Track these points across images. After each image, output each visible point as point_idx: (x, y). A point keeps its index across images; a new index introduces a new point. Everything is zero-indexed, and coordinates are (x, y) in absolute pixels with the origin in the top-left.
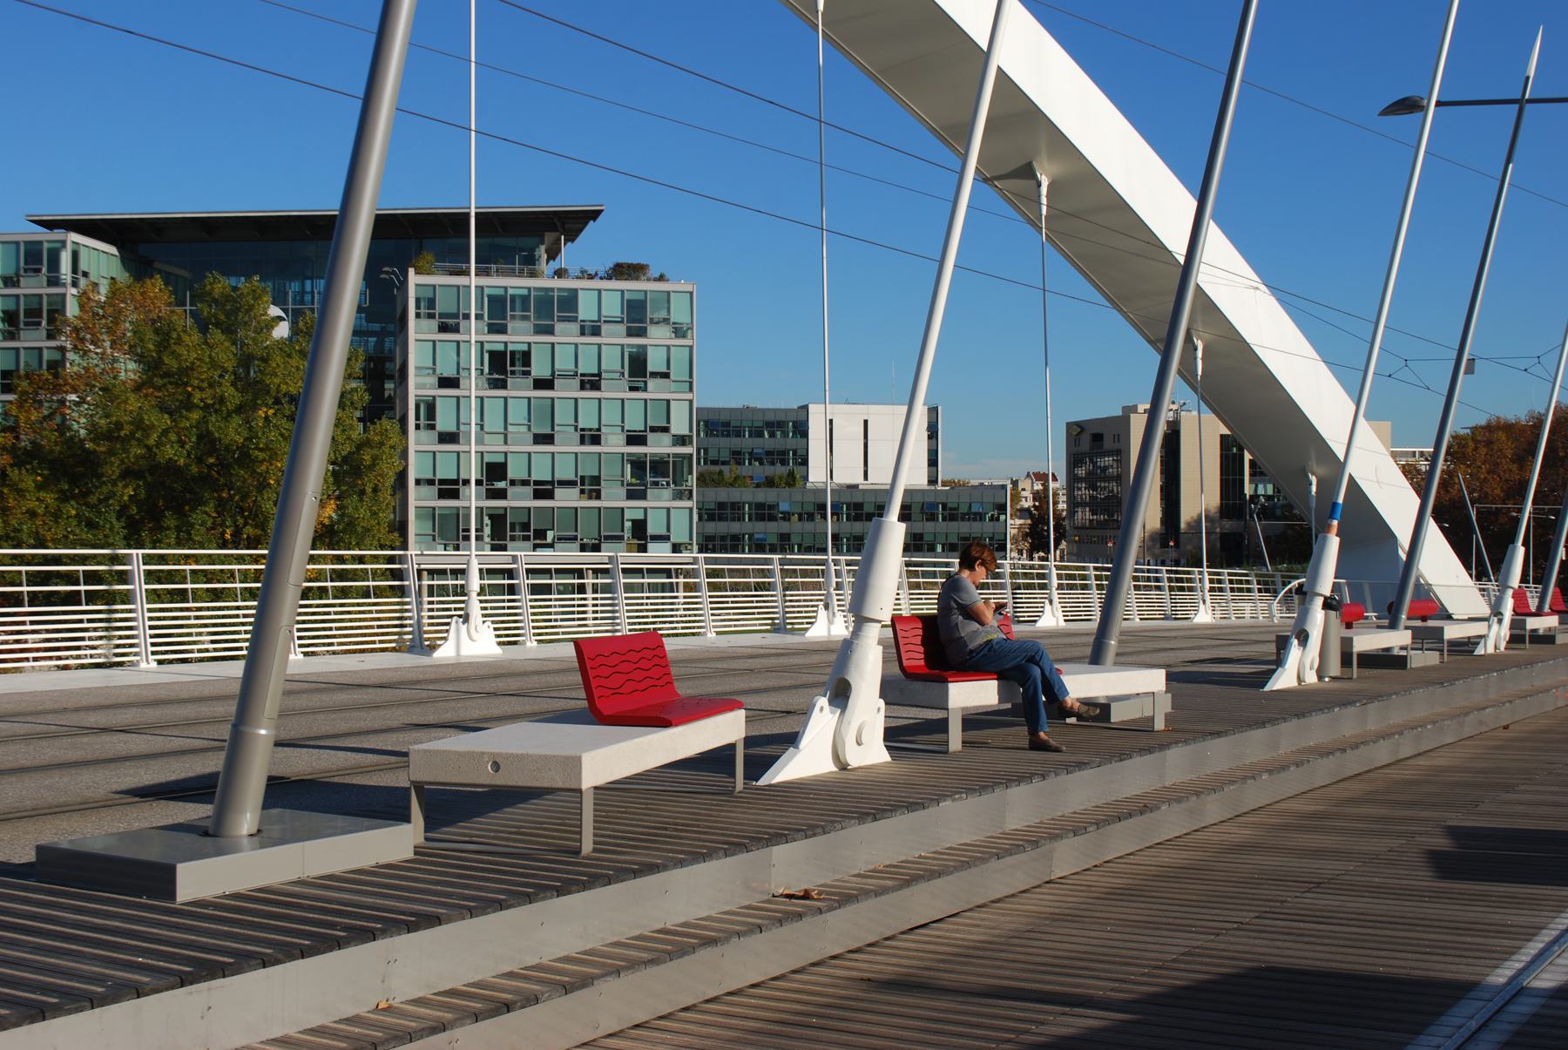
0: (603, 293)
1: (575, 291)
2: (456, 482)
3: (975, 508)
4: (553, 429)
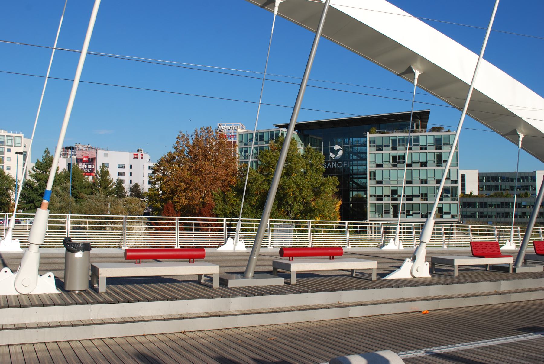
0: (428, 136)
1: (419, 136)
2: (382, 196)
4: (412, 179)
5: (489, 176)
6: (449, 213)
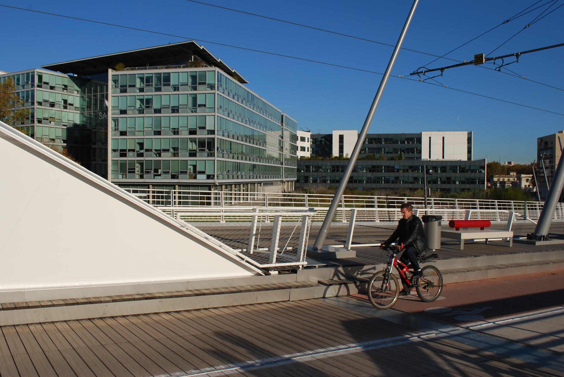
3: (472, 168)
5: (371, 137)
6: (203, 173)
